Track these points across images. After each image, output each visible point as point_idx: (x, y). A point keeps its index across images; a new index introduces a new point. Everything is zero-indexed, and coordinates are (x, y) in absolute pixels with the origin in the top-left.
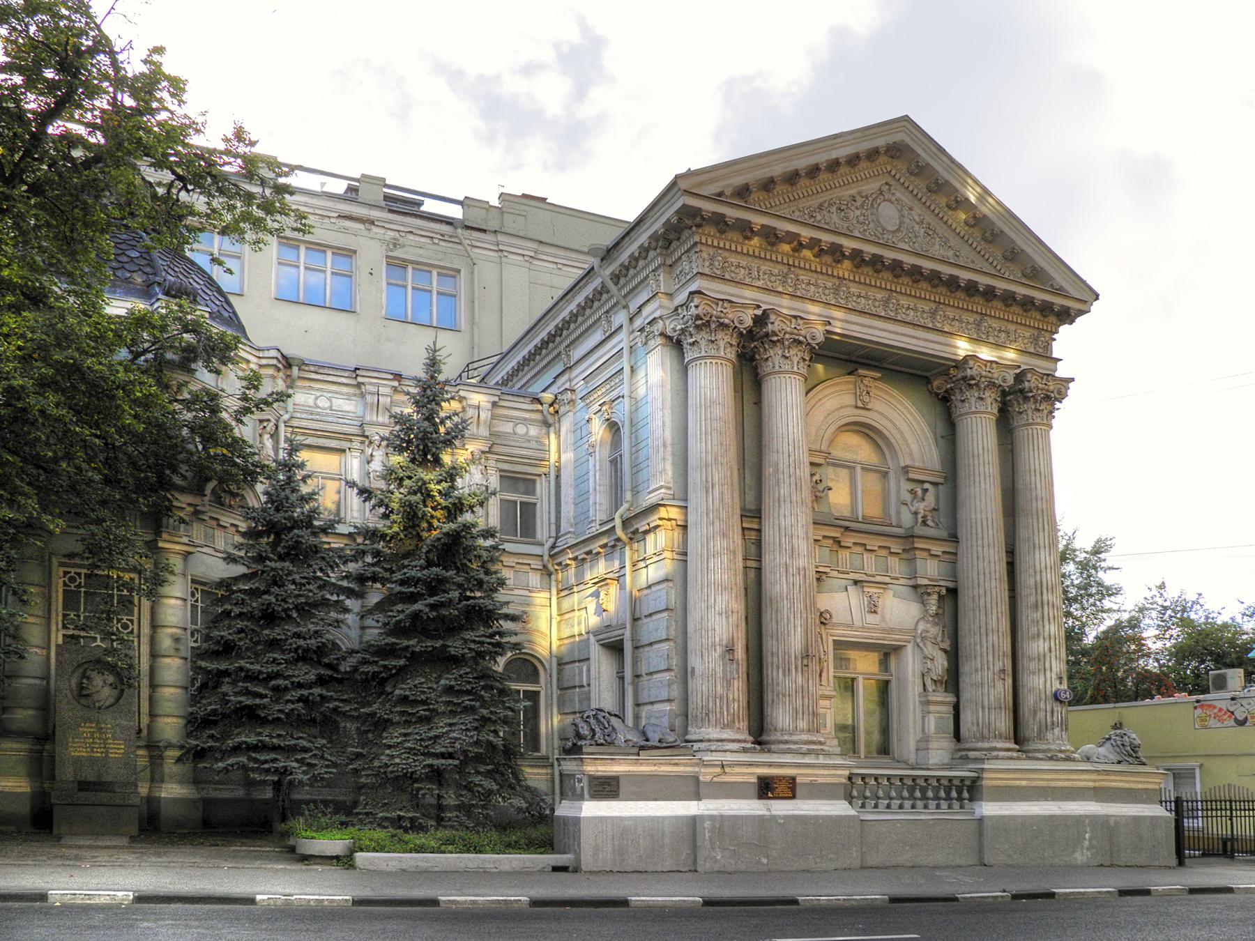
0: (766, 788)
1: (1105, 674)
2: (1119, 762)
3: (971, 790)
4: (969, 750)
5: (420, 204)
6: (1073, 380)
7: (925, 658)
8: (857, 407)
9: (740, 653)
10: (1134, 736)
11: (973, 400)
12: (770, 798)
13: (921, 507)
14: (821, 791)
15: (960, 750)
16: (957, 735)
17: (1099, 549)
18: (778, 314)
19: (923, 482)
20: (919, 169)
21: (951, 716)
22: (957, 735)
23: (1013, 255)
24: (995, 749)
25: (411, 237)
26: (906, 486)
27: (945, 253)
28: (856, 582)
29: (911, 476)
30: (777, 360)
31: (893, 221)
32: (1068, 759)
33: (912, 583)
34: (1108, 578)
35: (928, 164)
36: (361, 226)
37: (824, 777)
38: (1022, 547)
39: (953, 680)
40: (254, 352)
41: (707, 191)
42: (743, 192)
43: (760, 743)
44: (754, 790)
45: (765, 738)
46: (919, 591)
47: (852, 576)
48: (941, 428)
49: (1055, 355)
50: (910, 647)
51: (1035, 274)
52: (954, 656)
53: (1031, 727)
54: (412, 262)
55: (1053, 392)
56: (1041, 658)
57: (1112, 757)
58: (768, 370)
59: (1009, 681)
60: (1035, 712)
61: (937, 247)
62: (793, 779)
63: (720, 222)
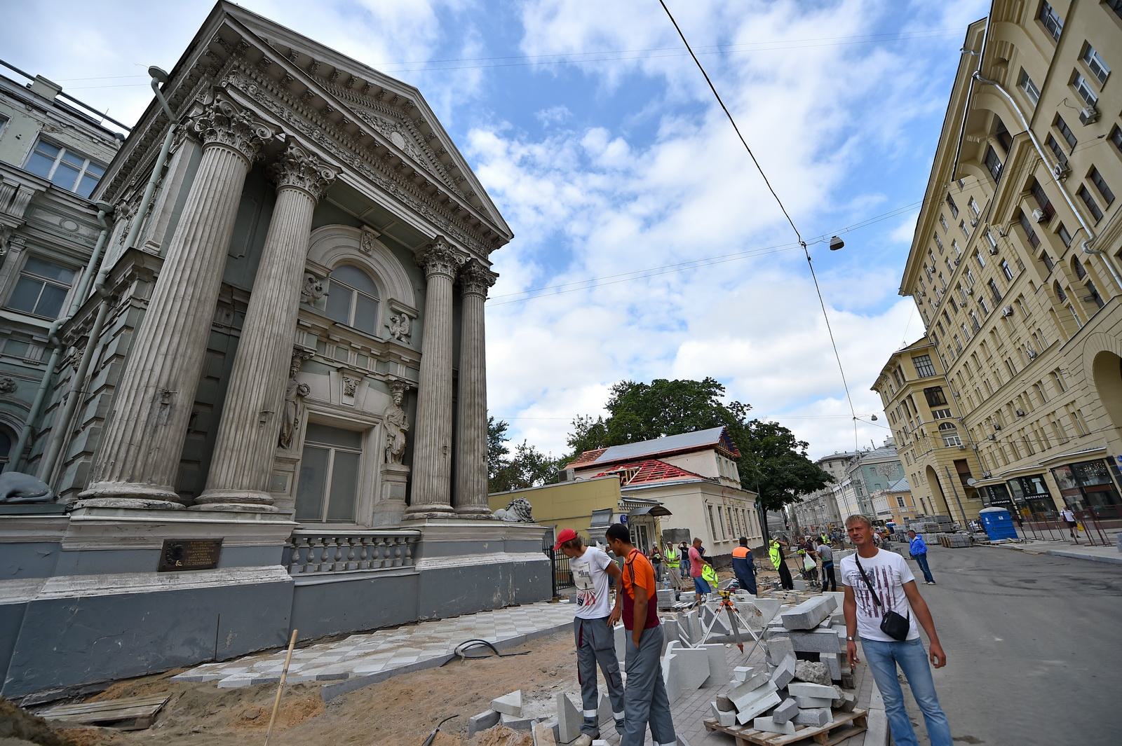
1: (506, 480)
2: (519, 521)
3: (415, 546)
4: (415, 512)
7: (388, 436)
8: (359, 250)
9: (183, 399)
10: (527, 502)
11: (440, 266)
14: (258, 558)
15: (409, 512)
16: (408, 501)
17: (501, 428)
22: (408, 501)
24: (435, 510)
26: (392, 315)
32: (489, 519)
33: (384, 379)
34: (504, 445)
38: (464, 367)
39: (406, 456)
46: (390, 386)
48: (418, 285)
50: (378, 427)
52: (410, 436)
53: (462, 493)
54: (67, 147)
56: (472, 442)
57: (514, 517)
59: (449, 456)
60: (466, 482)
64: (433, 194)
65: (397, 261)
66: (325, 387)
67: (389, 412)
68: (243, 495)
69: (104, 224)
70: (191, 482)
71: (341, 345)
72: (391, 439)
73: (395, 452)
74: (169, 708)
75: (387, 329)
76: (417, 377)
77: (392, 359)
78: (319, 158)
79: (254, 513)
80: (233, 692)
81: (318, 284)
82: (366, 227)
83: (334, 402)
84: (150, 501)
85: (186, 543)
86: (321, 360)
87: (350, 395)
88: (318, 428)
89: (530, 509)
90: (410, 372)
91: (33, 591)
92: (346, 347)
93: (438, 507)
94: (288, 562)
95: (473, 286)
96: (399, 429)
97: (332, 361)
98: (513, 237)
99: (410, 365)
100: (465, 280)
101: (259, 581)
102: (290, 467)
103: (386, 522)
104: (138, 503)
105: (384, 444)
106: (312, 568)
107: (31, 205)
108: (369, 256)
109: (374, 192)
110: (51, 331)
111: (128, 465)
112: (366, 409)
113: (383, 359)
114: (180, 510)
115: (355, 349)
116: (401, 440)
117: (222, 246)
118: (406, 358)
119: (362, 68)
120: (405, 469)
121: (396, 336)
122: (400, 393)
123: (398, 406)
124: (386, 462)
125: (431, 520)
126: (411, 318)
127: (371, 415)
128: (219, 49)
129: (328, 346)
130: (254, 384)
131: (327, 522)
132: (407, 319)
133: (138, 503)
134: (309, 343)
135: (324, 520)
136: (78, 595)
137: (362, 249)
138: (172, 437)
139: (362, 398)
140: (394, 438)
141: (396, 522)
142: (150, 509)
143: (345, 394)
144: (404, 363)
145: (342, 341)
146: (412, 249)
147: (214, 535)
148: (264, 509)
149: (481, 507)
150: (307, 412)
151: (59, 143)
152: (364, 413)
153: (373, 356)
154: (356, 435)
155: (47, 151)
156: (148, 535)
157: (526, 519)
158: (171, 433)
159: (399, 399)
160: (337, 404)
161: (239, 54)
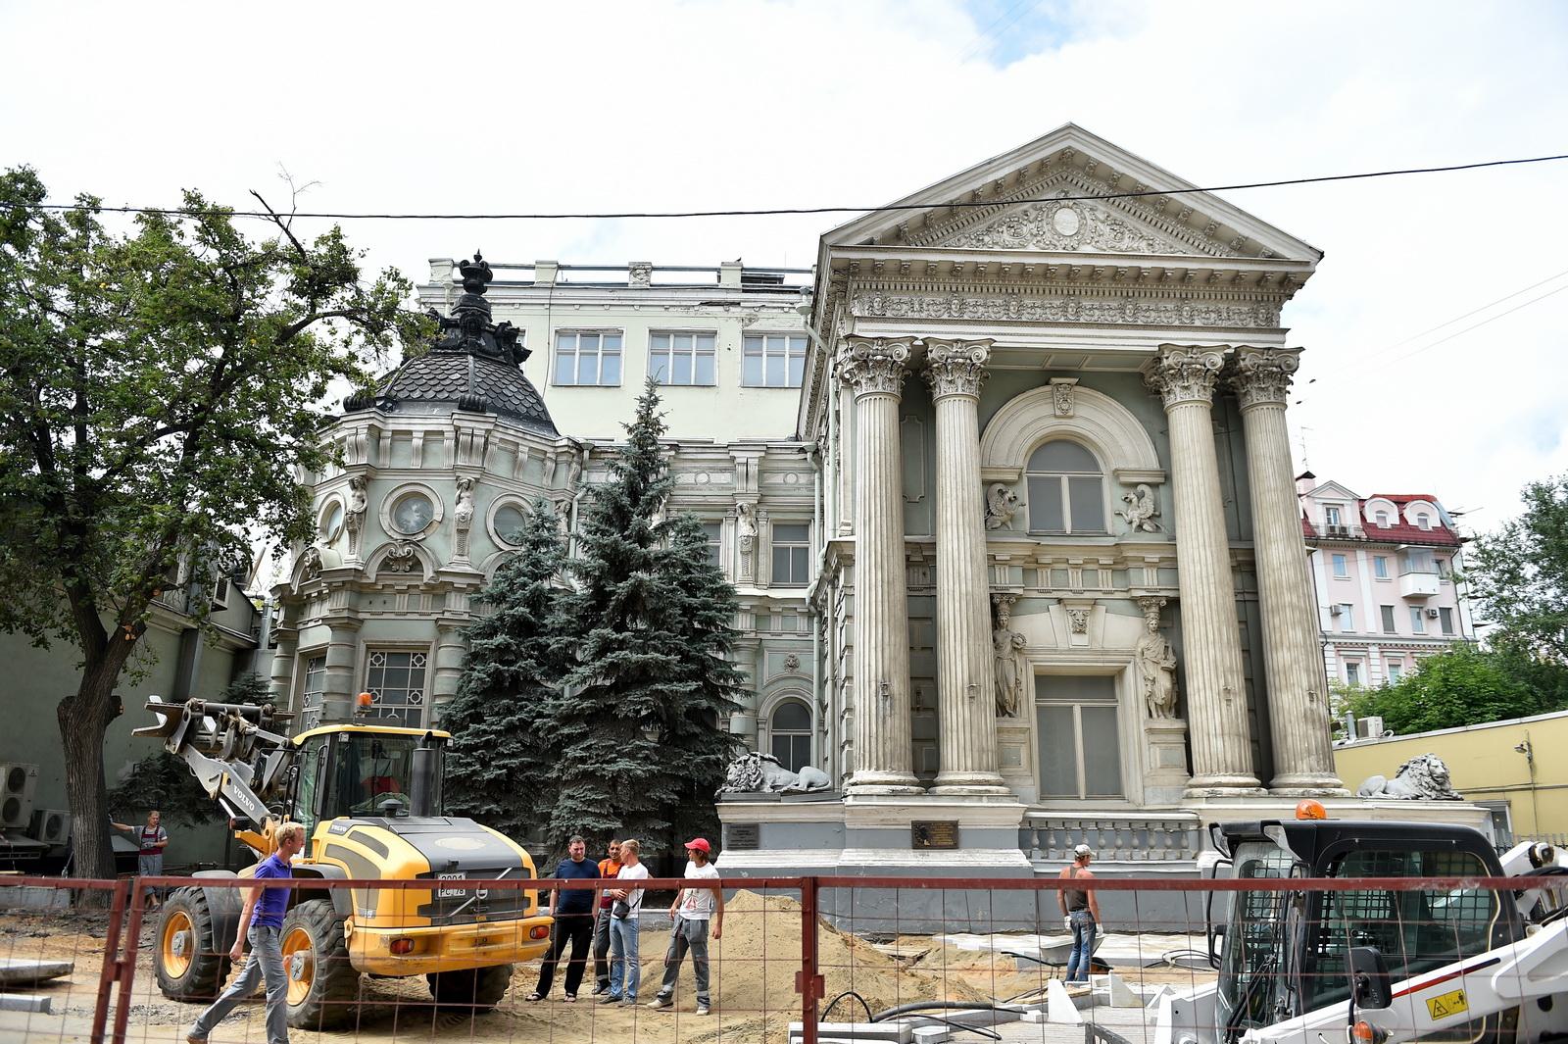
0: (924, 835)
2: (1417, 797)
5: (781, 280)
6: (1301, 349)
8: (1055, 416)
12: (927, 847)
13: (1134, 515)
14: (991, 839)
18: (937, 341)
19: (1136, 485)
20: (1092, 169)
21: (1183, 746)
23: (1213, 232)
25: (764, 310)
26: (1121, 492)
27: (1145, 246)
28: (1060, 601)
29: (1123, 479)
30: (943, 385)
31: (1072, 231)
35: (1099, 163)
36: (721, 308)
37: (992, 821)
39: (1179, 705)
40: (550, 443)
41: (853, 243)
42: (898, 236)
43: (1269, 787)
44: (909, 837)
45: (1274, 782)
47: (1055, 595)
49: (1282, 326)
51: (1242, 247)
52: (1178, 675)
54: (767, 333)
55: (1280, 370)
58: (936, 396)
61: (1126, 240)
62: (955, 825)
63: (876, 269)
64: (1138, 277)
65: (1114, 403)
66: (1045, 631)
67: (1143, 644)
68: (968, 777)
69: (815, 467)
70: (926, 768)
71: (1057, 566)
72: (1149, 683)
73: (1160, 702)
74: (928, 957)
75: (1120, 518)
76: (1177, 581)
77: (1131, 564)
78: (963, 341)
79: (979, 795)
80: (965, 953)
81: (1010, 495)
82: (1055, 380)
83: (1062, 646)
84: (893, 787)
85: (928, 824)
86: (1035, 594)
87: (1080, 630)
88: (1048, 682)
89: (1445, 776)
90: (1166, 576)
91: (837, 858)
92: (1064, 566)
93: (1224, 780)
94: (1024, 844)
95: (1254, 392)
96: (1159, 667)
97: (1049, 592)
98: (1322, 255)
99: (1161, 565)
100: (1239, 384)
101: (997, 864)
102: (1021, 737)
103: (1159, 800)
104: (885, 789)
105: (1143, 691)
106: (1054, 854)
107: (761, 472)
108: (1071, 417)
109: (1046, 336)
110: (807, 601)
111: (874, 756)
112: (1107, 646)
113: (1120, 567)
114: (919, 794)
115: (1076, 566)
116: (1165, 683)
117: (894, 514)
118: (1153, 557)
119: (983, 169)
120: (1179, 724)
121: (1134, 525)
122: (1153, 613)
123: (1156, 631)
124: (1151, 715)
125: (1211, 800)
126: (1153, 486)
127: (1117, 652)
128: (837, 277)
129: (1039, 574)
130: (960, 656)
131: (1087, 799)
132: (1147, 490)
133: (885, 789)
134: (1010, 580)
135: (1083, 797)
136: (863, 864)
137: (1058, 413)
138: (899, 725)
139: (1099, 632)
140: (1154, 681)
141: (1174, 800)
142: (894, 794)
143: (1074, 633)
144: (1151, 565)
145: (1056, 561)
146: (1137, 370)
147: (949, 817)
148: (989, 791)
149: (1313, 777)
150: (1030, 665)
151: (760, 332)
152: (1105, 652)
153: (1104, 567)
154: (1103, 683)
155: (753, 343)
156: (899, 817)
157: (1433, 794)
158: (897, 722)
159: (1154, 622)
160: (1066, 647)
161: (854, 274)
